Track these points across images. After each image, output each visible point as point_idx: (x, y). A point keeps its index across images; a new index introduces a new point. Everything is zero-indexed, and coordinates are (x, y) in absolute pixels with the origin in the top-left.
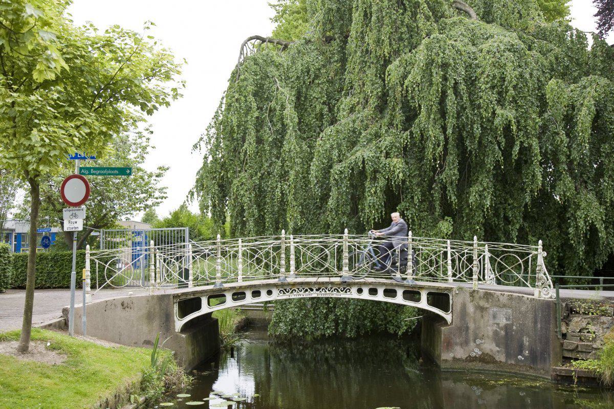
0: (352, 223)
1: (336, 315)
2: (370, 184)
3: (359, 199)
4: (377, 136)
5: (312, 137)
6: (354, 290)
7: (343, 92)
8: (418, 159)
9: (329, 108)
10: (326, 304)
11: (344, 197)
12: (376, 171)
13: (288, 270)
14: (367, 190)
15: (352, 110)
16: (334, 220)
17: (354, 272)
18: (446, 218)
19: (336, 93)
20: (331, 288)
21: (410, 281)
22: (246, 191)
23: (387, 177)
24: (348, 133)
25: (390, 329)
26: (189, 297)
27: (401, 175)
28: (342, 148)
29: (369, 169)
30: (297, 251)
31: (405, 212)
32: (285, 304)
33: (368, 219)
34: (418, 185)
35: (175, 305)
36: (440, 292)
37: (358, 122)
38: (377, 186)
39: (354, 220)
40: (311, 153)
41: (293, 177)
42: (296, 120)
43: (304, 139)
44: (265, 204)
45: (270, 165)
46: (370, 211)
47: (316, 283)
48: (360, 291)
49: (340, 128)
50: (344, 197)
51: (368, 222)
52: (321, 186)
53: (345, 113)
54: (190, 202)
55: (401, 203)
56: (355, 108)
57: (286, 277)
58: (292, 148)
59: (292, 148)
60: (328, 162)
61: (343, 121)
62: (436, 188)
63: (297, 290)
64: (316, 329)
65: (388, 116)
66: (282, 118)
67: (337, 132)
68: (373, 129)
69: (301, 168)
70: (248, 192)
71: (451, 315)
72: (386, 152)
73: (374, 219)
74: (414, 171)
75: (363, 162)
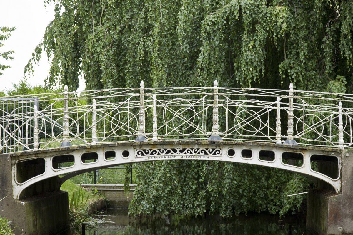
1: (207, 192)
2: (248, 37)
3: (235, 56)
6: (224, 151)
8: (307, 9)
10: (196, 179)
12: (254, 22)
14: (244, 44)
16: (206, 80)
18: (338, 77)
20: (198, 149)
21: (290, 141)
22: (103, 47)
25: (271, 209)
26: (30, 158)
27: (284, 26)
29: (246, 19)
31: (289, 71)
32: (149, 178)
33: (245, 78)
34: (305, 39)
35: (13, 168)
36: (326, 154)
39: (228, 80)
41: (157, 31)
44: (125, 63)
46: (247, 69)
48: (231, 153)
50: (217, 53)
54: (36, 61)
55: (284, 60)
62: (327, 42)
63: (158, 151)
64: (184, 208)
69: (167, 20)
70: (105, 49)
71: (339, 182)
74: (301, 22)
75: (240, 10)
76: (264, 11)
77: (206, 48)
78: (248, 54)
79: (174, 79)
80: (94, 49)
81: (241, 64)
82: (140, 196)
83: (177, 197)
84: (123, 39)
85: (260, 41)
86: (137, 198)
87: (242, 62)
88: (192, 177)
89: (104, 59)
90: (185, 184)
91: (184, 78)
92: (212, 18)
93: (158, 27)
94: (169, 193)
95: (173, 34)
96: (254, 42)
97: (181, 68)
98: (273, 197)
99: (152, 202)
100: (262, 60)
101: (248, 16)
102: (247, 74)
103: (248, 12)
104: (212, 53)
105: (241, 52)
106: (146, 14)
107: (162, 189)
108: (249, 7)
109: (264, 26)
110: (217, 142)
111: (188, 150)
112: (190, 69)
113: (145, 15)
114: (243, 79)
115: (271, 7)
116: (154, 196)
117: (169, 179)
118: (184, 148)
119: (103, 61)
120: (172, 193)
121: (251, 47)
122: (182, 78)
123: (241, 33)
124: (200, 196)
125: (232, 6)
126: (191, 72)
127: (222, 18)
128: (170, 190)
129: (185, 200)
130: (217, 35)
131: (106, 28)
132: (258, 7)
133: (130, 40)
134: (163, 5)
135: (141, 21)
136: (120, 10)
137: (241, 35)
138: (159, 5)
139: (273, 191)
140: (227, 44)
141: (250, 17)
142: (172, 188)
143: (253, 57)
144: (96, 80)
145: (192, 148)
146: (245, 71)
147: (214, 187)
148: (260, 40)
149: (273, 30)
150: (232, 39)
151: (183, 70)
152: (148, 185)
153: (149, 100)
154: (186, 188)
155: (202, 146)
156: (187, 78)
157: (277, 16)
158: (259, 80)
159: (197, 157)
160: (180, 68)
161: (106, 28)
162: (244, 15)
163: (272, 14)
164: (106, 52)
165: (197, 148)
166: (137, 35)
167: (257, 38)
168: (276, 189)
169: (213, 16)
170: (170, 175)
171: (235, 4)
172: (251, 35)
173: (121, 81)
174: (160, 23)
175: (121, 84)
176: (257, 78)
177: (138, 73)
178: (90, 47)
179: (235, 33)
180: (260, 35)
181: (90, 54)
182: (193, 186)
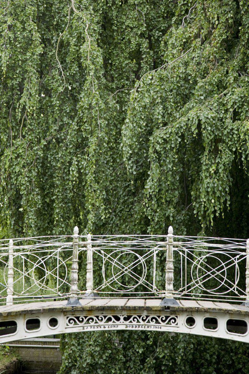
0: (180, 217)
1: (157, 358)
3: (193, 182)
4: (221, 86)
5: (123, 87)
6: (182, 320)
7: (174, 19)
9: (150, 43)
10: (143, 340)
11: (169, 179)
12: (217, 140)
13: (83, 287)
14: (204, 168)
15: (186, 46)
16: (156, 212)
17: (182, 291)
19: (161, 19)
20: (147, 317)
22: (24, 167)
23: (234, 150)
24: (178, 82)
28: (168, 104)
29: (207, 137)
30: (97, 260)
32: (83, 338)
33: (205, 212)
37: (192, 66)
38: (218, 163)
39: (183, 212)
40: (122, 112)
41: (94, 147)
42: (100, 60)
43: (112, 90)
45: (61, 128)
46: (208, 200)
47: (124, 309)
48: (191, 322)
49: (165, 73)
50: (169, 179)
51: (204, 217)
52: (137, 162)
53: (175, 51)
56: (191, 43)
57: (79, 299)
58: (94, 103)
59: (94, 103)
60: (147, 125)
61: (171, 64)
63: (95, 318)
65: (240, 56)
66: (79, 58)
67: (161, 79)
68: (214, 76)
69: (107, 133)
70: (26, 169)
72: (234, 111)
73: (215, 211)
75: (199, 126)
76: (230, 127)
77: (156, 172)
78: (209, 181)
79: (113, 208)
80: (12, 169)
81: (200, 193)
82: (72, 362)
83: (118, 365)
84: (49, 156)
85: (224, 165)
86: (67, 364)
87: (201, 190)
88: (137, 337)
89: (24, 182)
90: (128, 346)
91: (126, 206)
92: (163, 135)
93: (95, 143)
94: (107, 359)
95: (114, 148)
96: (217, 166)
97: (122, 194)
98: (241, 366)
99: (85, 372)
100: (227, 190)
101: (209, 133)
102: (208, 206)
103: (209, 128)
104: (163, 178)
105: (200, 178)
106: (79, 124)
107: (99, 354)
108: (210, 121)
109: (230, 145)
110: (172, 308)
111: (135, 318)
112: (134, 194)
113: (77, 126)
114: (202, 212)
115: (239, 121)
116: (88, 364)
117: (108, 340)
118: (129, 315)
119: (24, 185)
120: (112, 359)
121: (212, 172)
122: (124, 207)
123: (200, 153)
124: (148, 364)
125: (189, 119)
126: (135, 199)
127: (177, 135)
128: (110, 355)
129: (129, 369)
130: (170, 156)
131: (28, 142)
132: (221, 120)
133: (59, 158)
134: (101, 115)
135: (73, 134)
136: (46, 119)
137: (200, 157)
138: (96, 115)
139: (241, 358)
140: (181, 165)
141: (212, 134)
142: (112, 353)
143: (216, 185)
144: (13, 208)
145: (139, 315)
146: (205, 202)
147: (166, 352)
148: (224, 163)
149: (241, 151)
150: (188, 160)
151: (125, 196)
152: (82, 347)
153: (83, 235)
154: (129, 352)
155: (152, 313)
156: (130, 206)
157: (246, 133)
158: (223, 214)
159: (146, 327)
160: (121, 193)
161: (28, 142)
162: (204, 132)
163: (240, 130)
164: (27, 173)
165: (146, 314)
166: (68, 151)
167: (221, 160)
168: (245, 355)
169: (165, 132)
170: (109, 335)
171: (193, 118)
172: (213, 156)
173: (46, 209)
174: (97, 138)
175: (46, 213)
176: (220, 211)
177: (69, 199)
178: (6, 167)
179: (192, 152)
180: (224, 157)
181: (6, 175)
182: (139, 349)
